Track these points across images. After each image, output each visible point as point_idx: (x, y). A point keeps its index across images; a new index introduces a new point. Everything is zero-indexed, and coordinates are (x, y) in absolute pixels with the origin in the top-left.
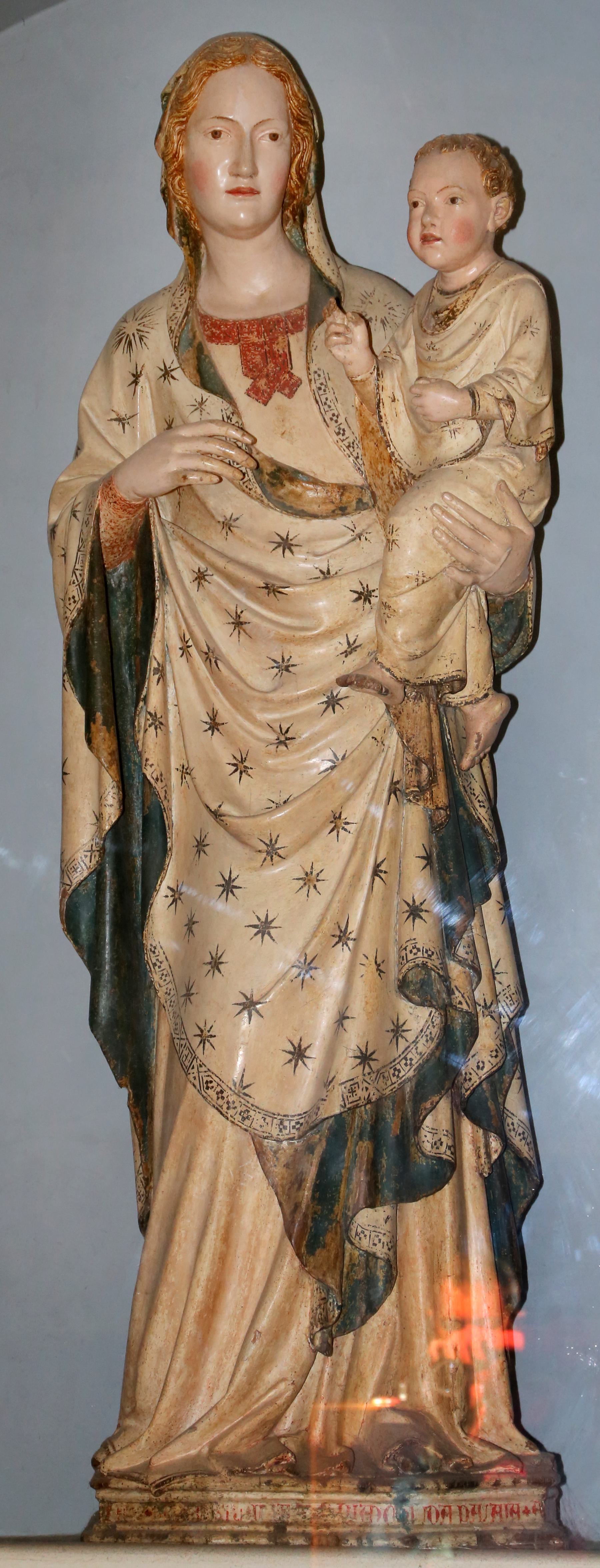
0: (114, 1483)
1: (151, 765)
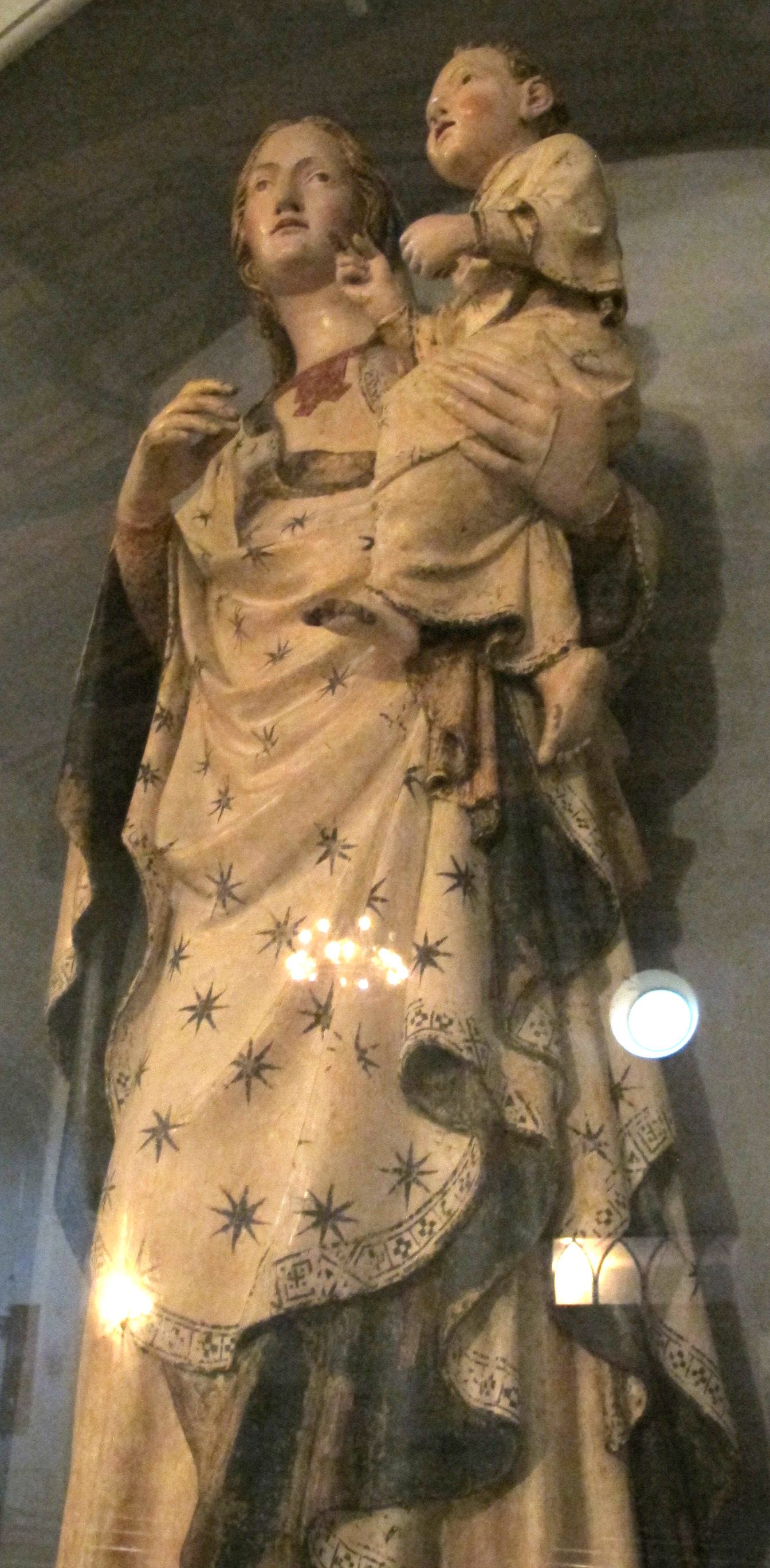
1: (132, 826)
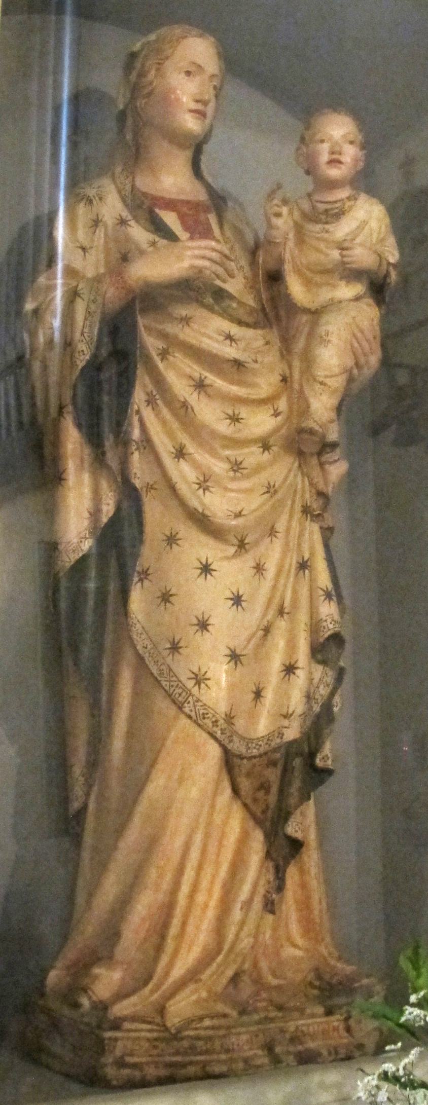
0: (127, 1025)
